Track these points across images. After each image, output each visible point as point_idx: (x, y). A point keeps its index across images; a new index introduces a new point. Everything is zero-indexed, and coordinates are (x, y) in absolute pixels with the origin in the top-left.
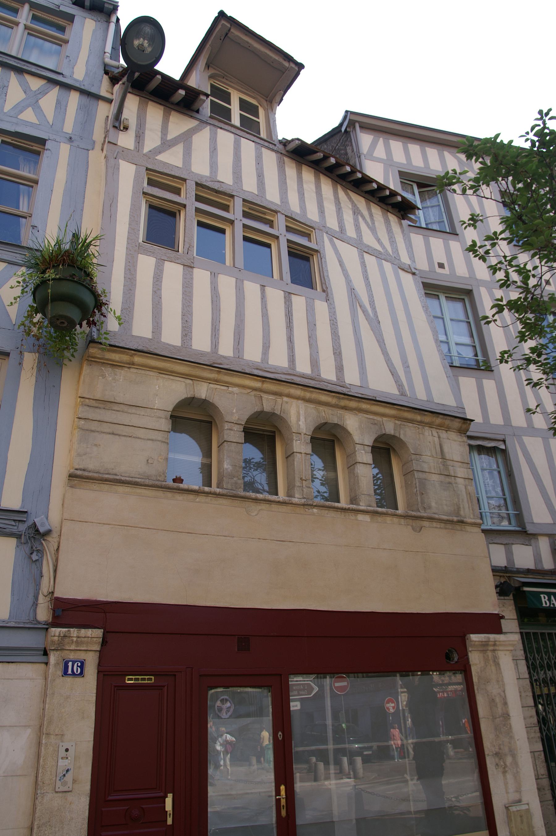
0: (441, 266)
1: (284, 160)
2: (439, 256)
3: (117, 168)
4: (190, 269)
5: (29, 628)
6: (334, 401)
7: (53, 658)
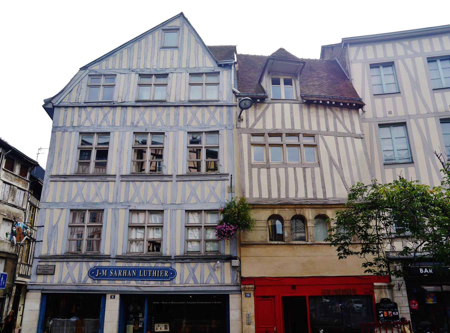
0: (390, 113)
1: (302, 106)
2: (389, 107)
3: (241, 137)
4: (269, 169)
5: (236, 286)
6: (321, 207)
7: (243, 293)
